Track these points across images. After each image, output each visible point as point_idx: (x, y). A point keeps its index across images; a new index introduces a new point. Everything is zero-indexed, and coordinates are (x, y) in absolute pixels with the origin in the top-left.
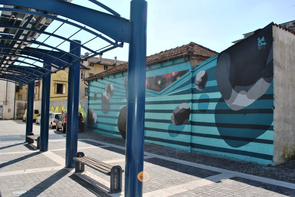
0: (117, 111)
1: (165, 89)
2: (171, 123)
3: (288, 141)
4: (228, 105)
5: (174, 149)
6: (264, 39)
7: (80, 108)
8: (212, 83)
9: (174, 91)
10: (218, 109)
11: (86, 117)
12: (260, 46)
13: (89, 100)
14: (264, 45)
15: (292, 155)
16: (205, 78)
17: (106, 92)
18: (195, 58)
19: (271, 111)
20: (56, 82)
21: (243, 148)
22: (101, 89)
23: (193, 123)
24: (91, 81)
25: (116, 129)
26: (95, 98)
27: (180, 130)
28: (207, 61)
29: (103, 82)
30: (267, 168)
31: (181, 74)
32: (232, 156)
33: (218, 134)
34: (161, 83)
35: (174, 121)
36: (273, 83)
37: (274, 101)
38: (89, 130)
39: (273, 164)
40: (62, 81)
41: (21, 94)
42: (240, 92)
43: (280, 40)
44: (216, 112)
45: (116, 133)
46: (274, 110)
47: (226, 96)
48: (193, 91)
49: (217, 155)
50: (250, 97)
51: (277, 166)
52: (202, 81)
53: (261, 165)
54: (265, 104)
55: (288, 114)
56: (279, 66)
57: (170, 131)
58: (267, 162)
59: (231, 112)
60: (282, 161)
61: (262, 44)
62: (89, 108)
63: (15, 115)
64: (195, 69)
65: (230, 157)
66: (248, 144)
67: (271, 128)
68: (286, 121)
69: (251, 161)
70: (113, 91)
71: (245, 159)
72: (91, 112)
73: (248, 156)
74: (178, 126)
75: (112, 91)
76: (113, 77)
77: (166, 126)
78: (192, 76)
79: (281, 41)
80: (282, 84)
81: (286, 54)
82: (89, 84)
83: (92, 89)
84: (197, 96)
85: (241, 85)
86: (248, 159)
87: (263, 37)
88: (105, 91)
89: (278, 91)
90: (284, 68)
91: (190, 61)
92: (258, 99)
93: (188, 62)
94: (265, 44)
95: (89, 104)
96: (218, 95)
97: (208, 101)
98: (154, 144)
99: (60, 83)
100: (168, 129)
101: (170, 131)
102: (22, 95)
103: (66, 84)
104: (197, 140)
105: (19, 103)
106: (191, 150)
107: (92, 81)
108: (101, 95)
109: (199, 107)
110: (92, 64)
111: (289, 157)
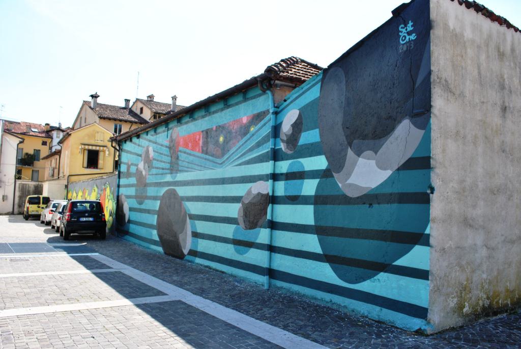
0: (155, 198)
1: (231, 152)
2: (238, 224)
3: (473, 271)
4: (340, 185)
5: (241, 280)
6: (412, 26)
7: (109, 194)
8: (310, 137)
9: (243, 157)
10: (320, 193)
11: (115, 212)
12: (403, 44)
13: (119, 177)
14: (412, 40)
15: (483, 305)
16: (298, 127)
17: (143, 162)
18: (283, 83)
19: (423, 198)
20: (87, 147)
21: (365, 286)
22: (136, 156)
23: (273, 225)
24: (124, 142)
25: (155, 235)
26: (129, 175)
27: (252, 240)
28: (302, 88)
29: (140, 144)
30: (411, 341)
31: (258, 118)
32: (345, 304)
33: (318, 250)
34: (224, 141)
35: (242, 219)
36: (430, 128)
37: (432, 175)
38: (118, 237)
39: (429, 330)
40: (96, 146)
41: (37, 169)
42: (362, 155)
43: (452, 28)
44: (318, 200)
45: (154, 243)
46: (431, 195)
47: (337, 164)
48: (276, 156)
49: (316, 299)
50: (382, 166)
51: (440, 334)
52: (292, 133)
53: (401, 329)
54: (411, 182)
55: (474, 206)
56: (447, 88)
57: (236, 242)
58: (416, 323)
59: (345, 200)
60: (454, 321)
61: (408, 37)
62: (120, 194)
63: (16, 207)
64: (280, 109)
65: (340, 305)
66: (375, 278)
67: (421, 239)
68: (467, 223)
69: (381, 317)
70: (151, 159)
71: (369, 313)
72: (121, 201)
73: (374, 306)
74: (249, 231)
75: (151, 160)
76: (152, 132)
77: (228, 231)
78: (276, 124)
79: (454, 29)
80: (457, 133)
81: (469, 62)
82: (120, 148)
83: (125, 158)
84: (284, 167)
85: (364, 137)
86: (363, 308)
87: (410, 22)
88: (142, 161)
89: (444, 151)
90: (462, 95)
91: (270, 90)
92: (398, 169)
93: (268, 92)
94: (413, 37)
95: (119, 186)
96: (320, 163)
97: (301, 175)
98: (210, 268)
99: (94, 148)
100: (232, 237)
101: (236, 242)
102: (38, 171)
103: (104, 151)
104: (283, 263)
105: (24, 184)
106: (270, 285)
107: (125, 142)
108: (136, 167)
109: (286, 189)
110: (158, 115)
111: (476, 310)
